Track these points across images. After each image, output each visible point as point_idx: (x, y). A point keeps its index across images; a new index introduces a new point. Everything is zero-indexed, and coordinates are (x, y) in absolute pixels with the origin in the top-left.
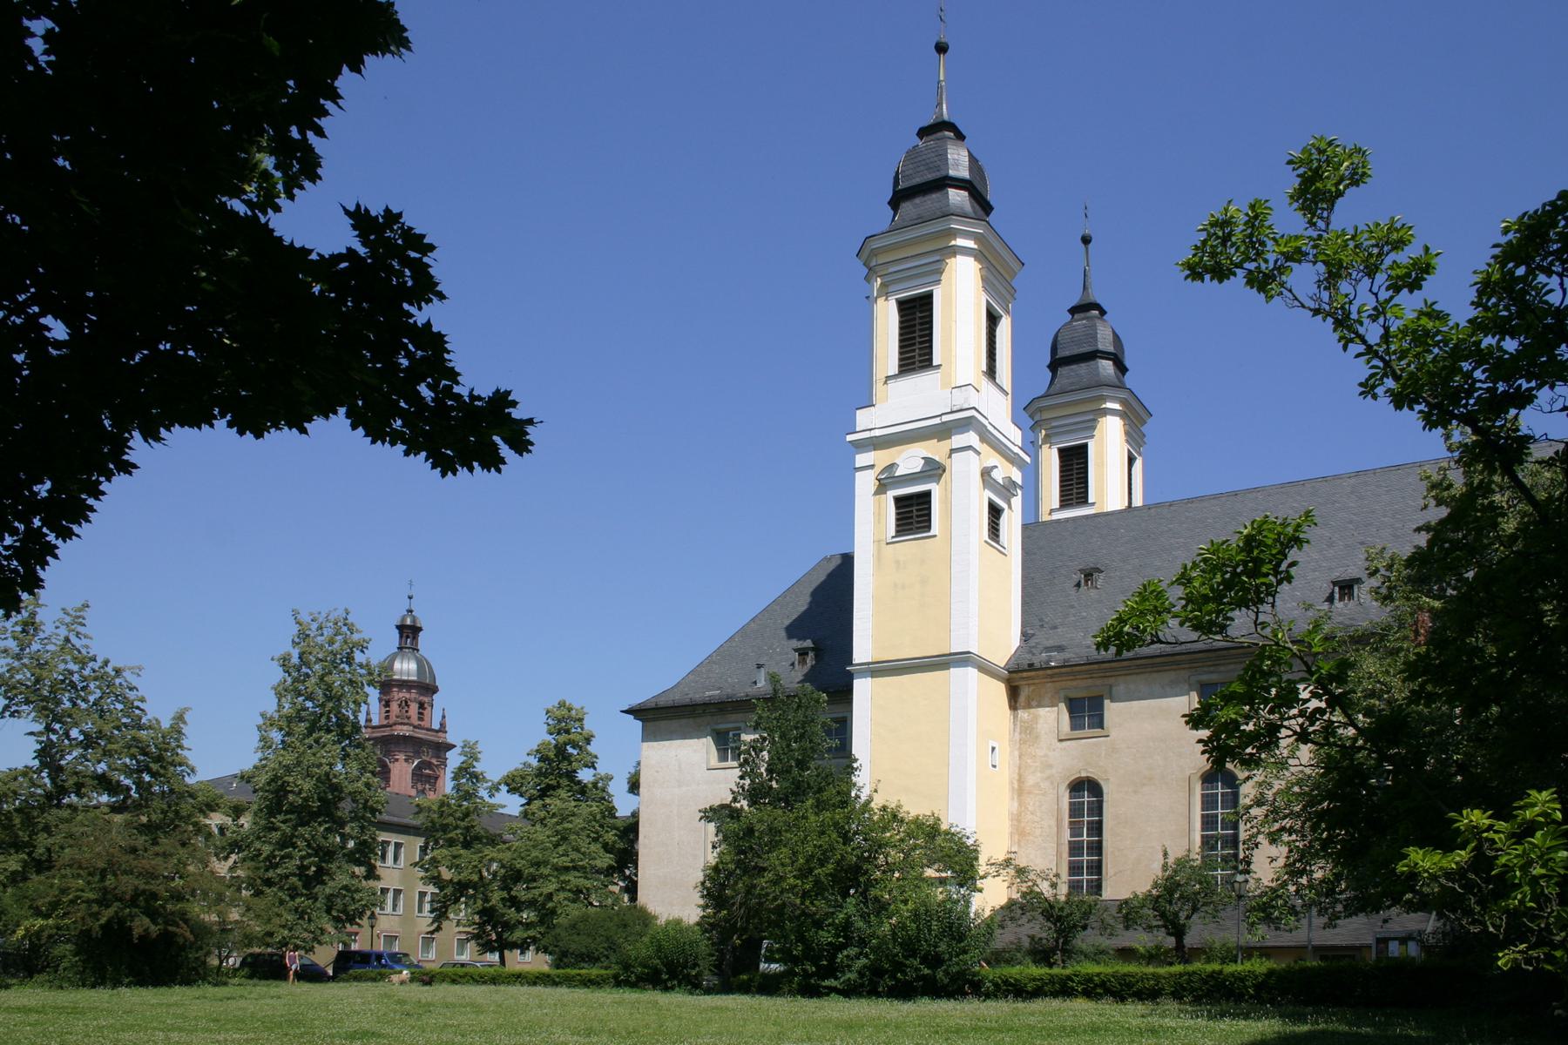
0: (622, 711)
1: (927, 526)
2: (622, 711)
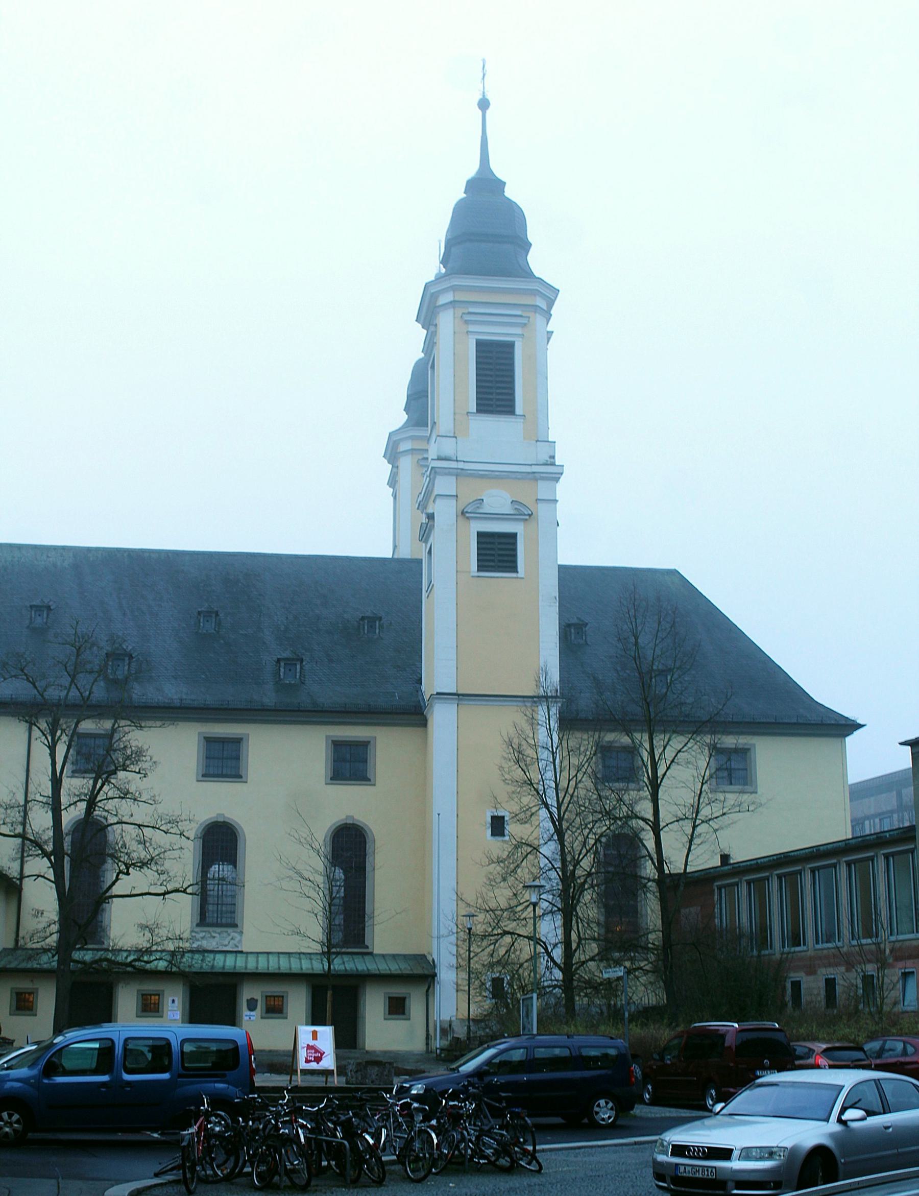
0: (901, 744)
1: (513, 568)
2: (901, 744)
